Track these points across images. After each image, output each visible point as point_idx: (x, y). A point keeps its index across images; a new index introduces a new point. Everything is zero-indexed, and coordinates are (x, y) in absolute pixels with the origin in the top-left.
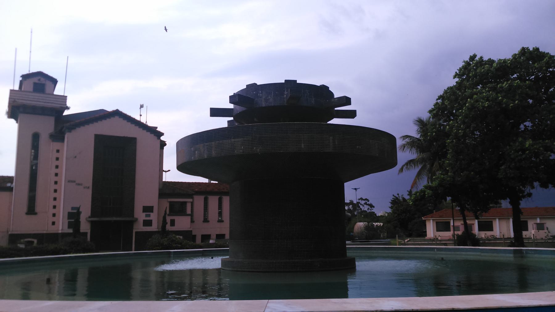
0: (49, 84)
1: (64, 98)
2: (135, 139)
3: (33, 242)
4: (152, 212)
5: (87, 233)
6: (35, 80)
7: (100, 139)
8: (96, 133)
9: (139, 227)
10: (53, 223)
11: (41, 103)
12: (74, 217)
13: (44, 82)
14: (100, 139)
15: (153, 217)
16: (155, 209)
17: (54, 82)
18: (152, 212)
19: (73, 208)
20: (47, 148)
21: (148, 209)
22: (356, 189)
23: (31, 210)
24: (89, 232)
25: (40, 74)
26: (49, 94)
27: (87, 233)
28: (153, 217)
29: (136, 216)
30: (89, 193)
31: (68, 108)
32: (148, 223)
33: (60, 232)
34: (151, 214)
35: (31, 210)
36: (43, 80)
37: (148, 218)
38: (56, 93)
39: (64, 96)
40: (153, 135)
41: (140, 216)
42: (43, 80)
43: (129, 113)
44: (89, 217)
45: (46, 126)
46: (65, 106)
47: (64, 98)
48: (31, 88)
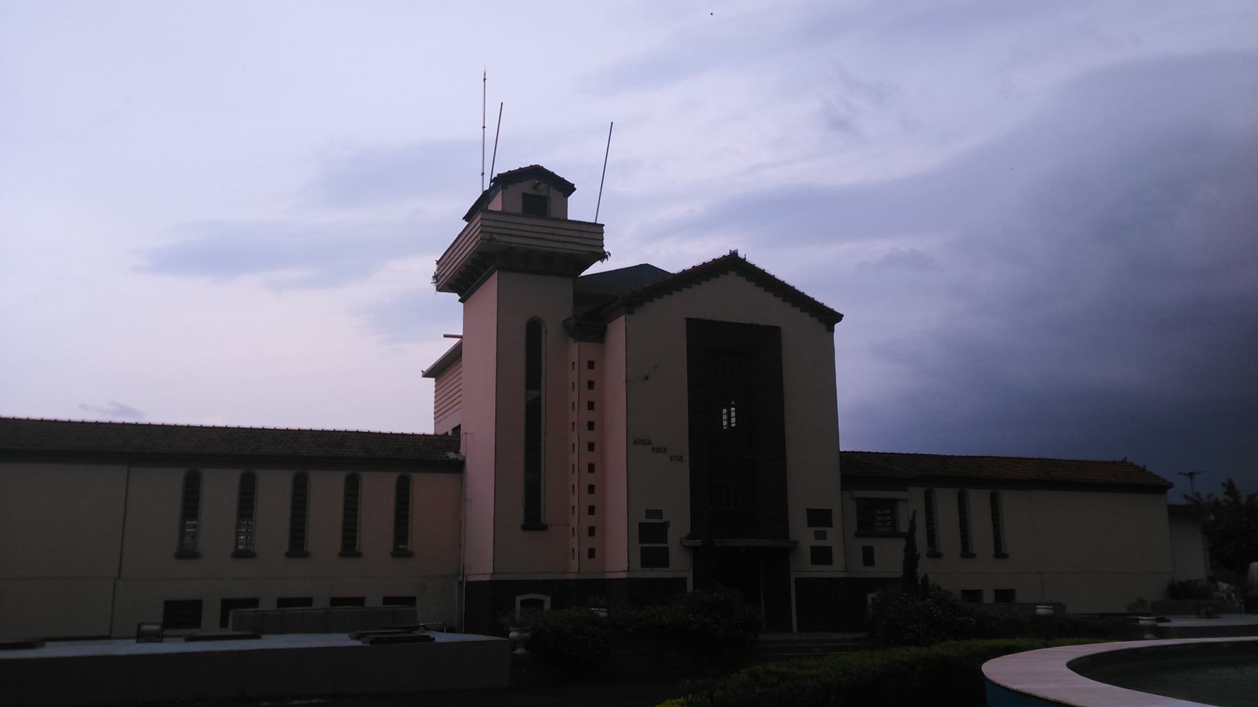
0: (554, 194)
1: (596, 230)
2: (776, 331)
3: (541, 603)
4: (830, 525)
5: (684, 580)
6: (526, 187)
7: (698, 330)
8: (693, 315)
9: (803, 567)
10: (592, 553)
11: (549, 244)
12: (651, 533)
13: (544, 193)
14: (698, 330)
15: (833, 538)
16: (836, 518)
17: (569, 188)
18: (830, 525)
19: (649, 513)
20: (565, 358)
21: (819, 518)
22: (1191, 475)
23: (533, 521)
24: (689, 576)
25: (536, 173)
26: (557, 220)
27: (684, 580)
28: (833, 538)
29: (793, 536)
30: (682, 472)
31: (603, 256)
32: (822, 555)
33: (572, 577)
34: (827, 529)
35: (533, 521)
36: (543, 189)
37: (821, 543)
38: (572, 215)
39: (595, 224)
40: (816, 319)
41: (803, 536)
42: (543, 189)
43: (760, 264)
44: (688, 538)
45: (553, 303)
46: (597, 250)
47: (596, 230)
48: (517, 206)
